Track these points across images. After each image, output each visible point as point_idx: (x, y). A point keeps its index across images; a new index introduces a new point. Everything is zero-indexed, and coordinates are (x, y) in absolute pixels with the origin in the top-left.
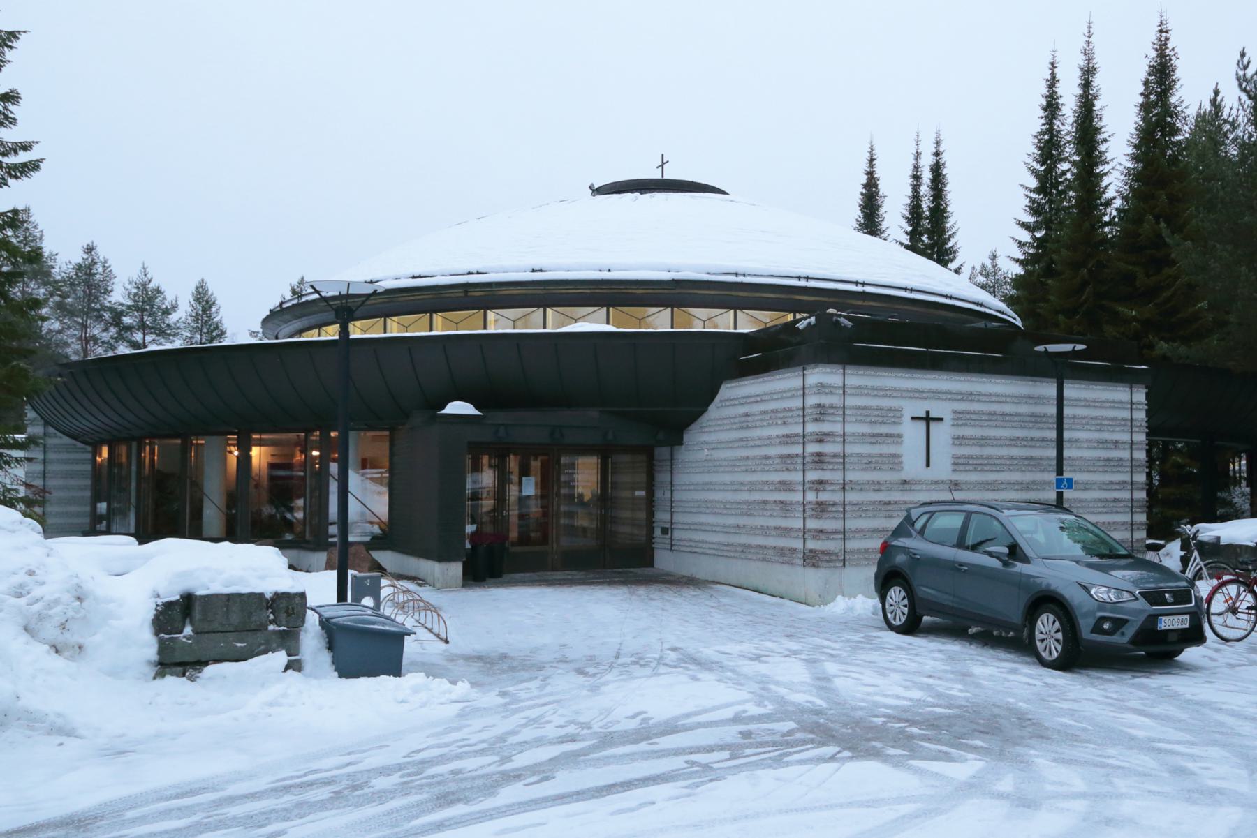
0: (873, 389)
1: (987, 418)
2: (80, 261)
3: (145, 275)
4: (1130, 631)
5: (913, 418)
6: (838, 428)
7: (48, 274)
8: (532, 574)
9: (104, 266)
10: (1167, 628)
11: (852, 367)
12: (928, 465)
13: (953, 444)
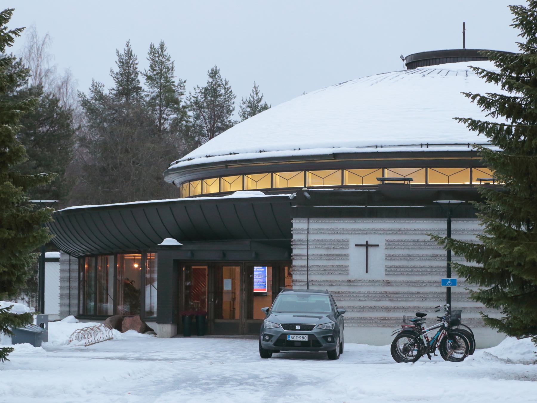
0: (327, 230)
1: (412, 243)
2: (205, 85)
3: (257, 94)
4: (274, 339)
5: (356, 245)
6: (304, 252)
7: (177, 102)
8: (254, 336)
9: (225, 88)
10: (293, 340)
11: (312, 219)
12: (367, 272)
13: (386, 259)
